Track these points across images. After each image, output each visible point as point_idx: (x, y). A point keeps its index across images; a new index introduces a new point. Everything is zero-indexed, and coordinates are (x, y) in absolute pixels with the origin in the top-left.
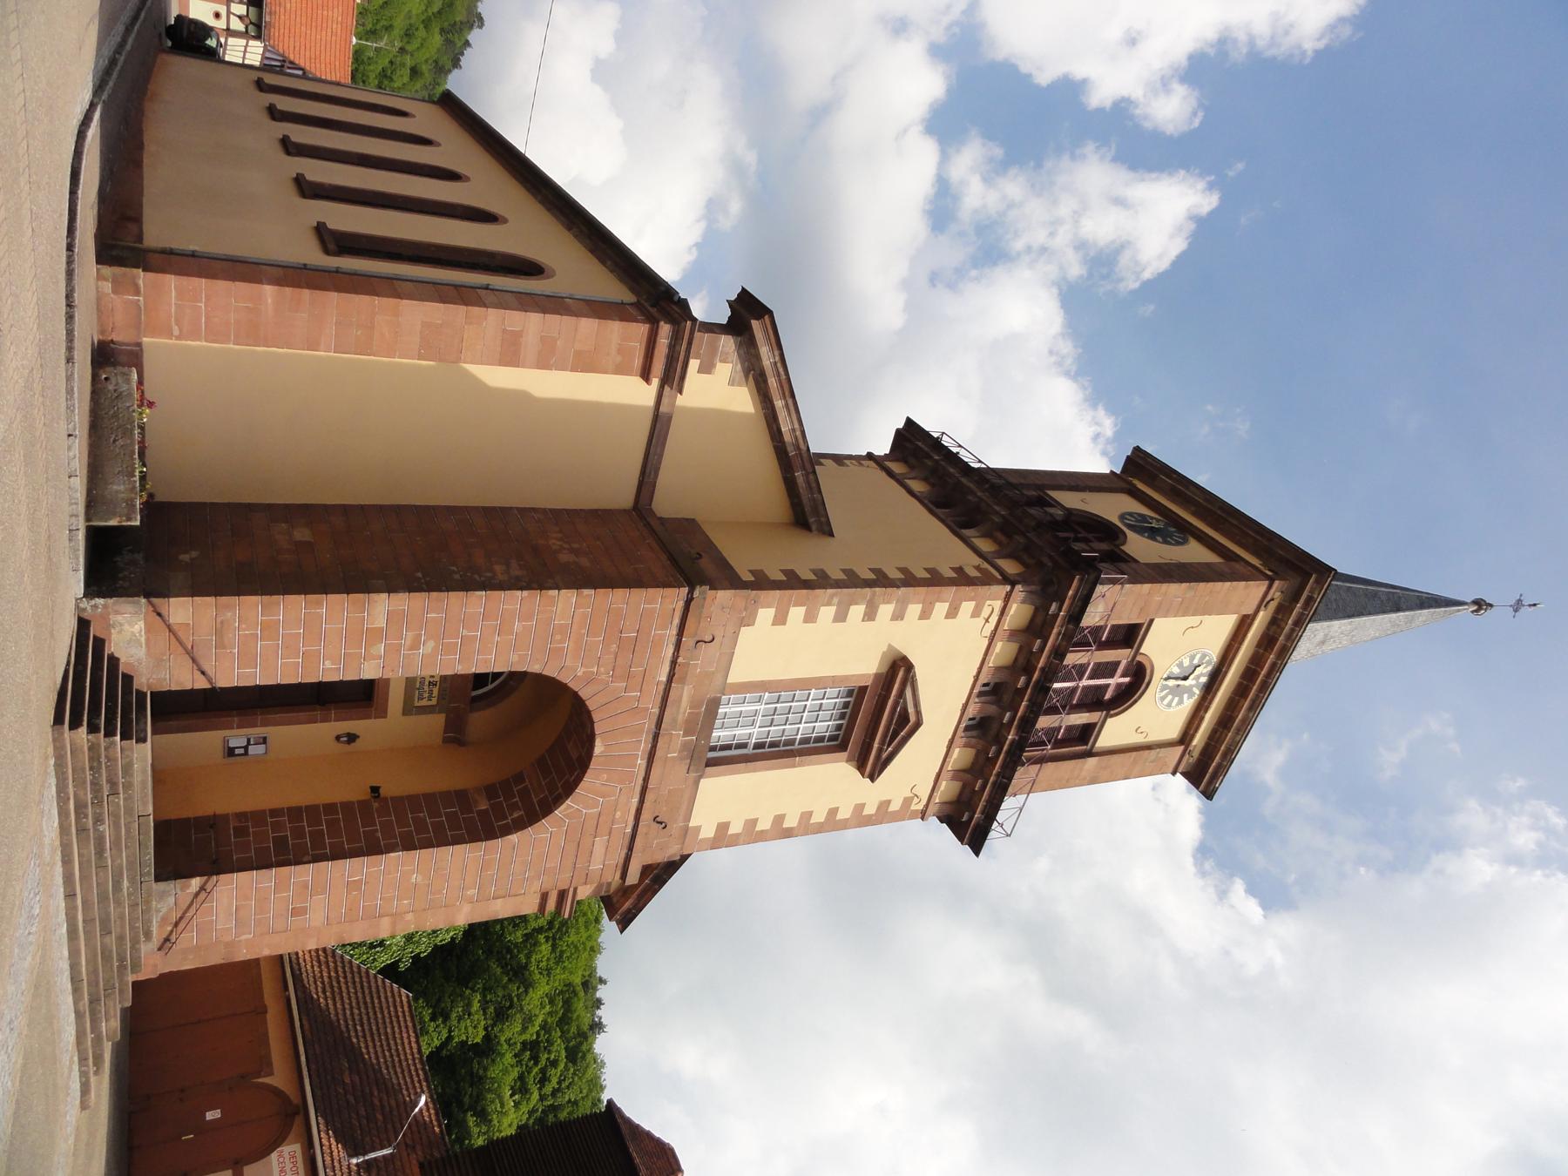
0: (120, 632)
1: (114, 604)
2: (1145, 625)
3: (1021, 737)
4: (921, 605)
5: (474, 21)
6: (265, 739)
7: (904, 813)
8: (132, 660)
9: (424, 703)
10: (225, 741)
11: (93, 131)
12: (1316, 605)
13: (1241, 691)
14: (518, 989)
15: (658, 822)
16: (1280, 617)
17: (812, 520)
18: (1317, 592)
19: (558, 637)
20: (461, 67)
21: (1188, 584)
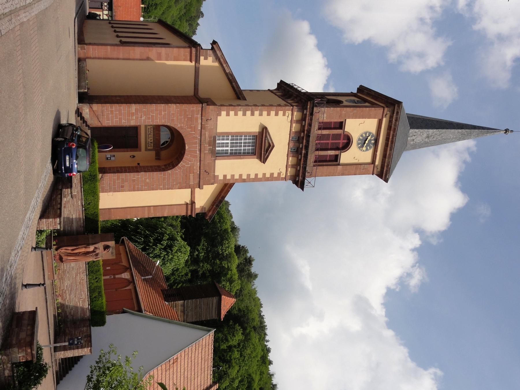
0: (84, 112)
1: (84, 105)
2: (344, 122)
3: (306, 152)
4: (266, 112)
5: (200, 15)
6: (114, 155)
7: (278, 178)
8: (87, 118)
9: (150, 148)
10: (106, 156)
11: (76, 20)
12: (399, 114)
13: (386, 145)
14: (226, 365)
16: (391, 120)
17: (240, 96)
18: (399, 110)
19: (173, 116)
20: (196, 34)
21: (353, 108)
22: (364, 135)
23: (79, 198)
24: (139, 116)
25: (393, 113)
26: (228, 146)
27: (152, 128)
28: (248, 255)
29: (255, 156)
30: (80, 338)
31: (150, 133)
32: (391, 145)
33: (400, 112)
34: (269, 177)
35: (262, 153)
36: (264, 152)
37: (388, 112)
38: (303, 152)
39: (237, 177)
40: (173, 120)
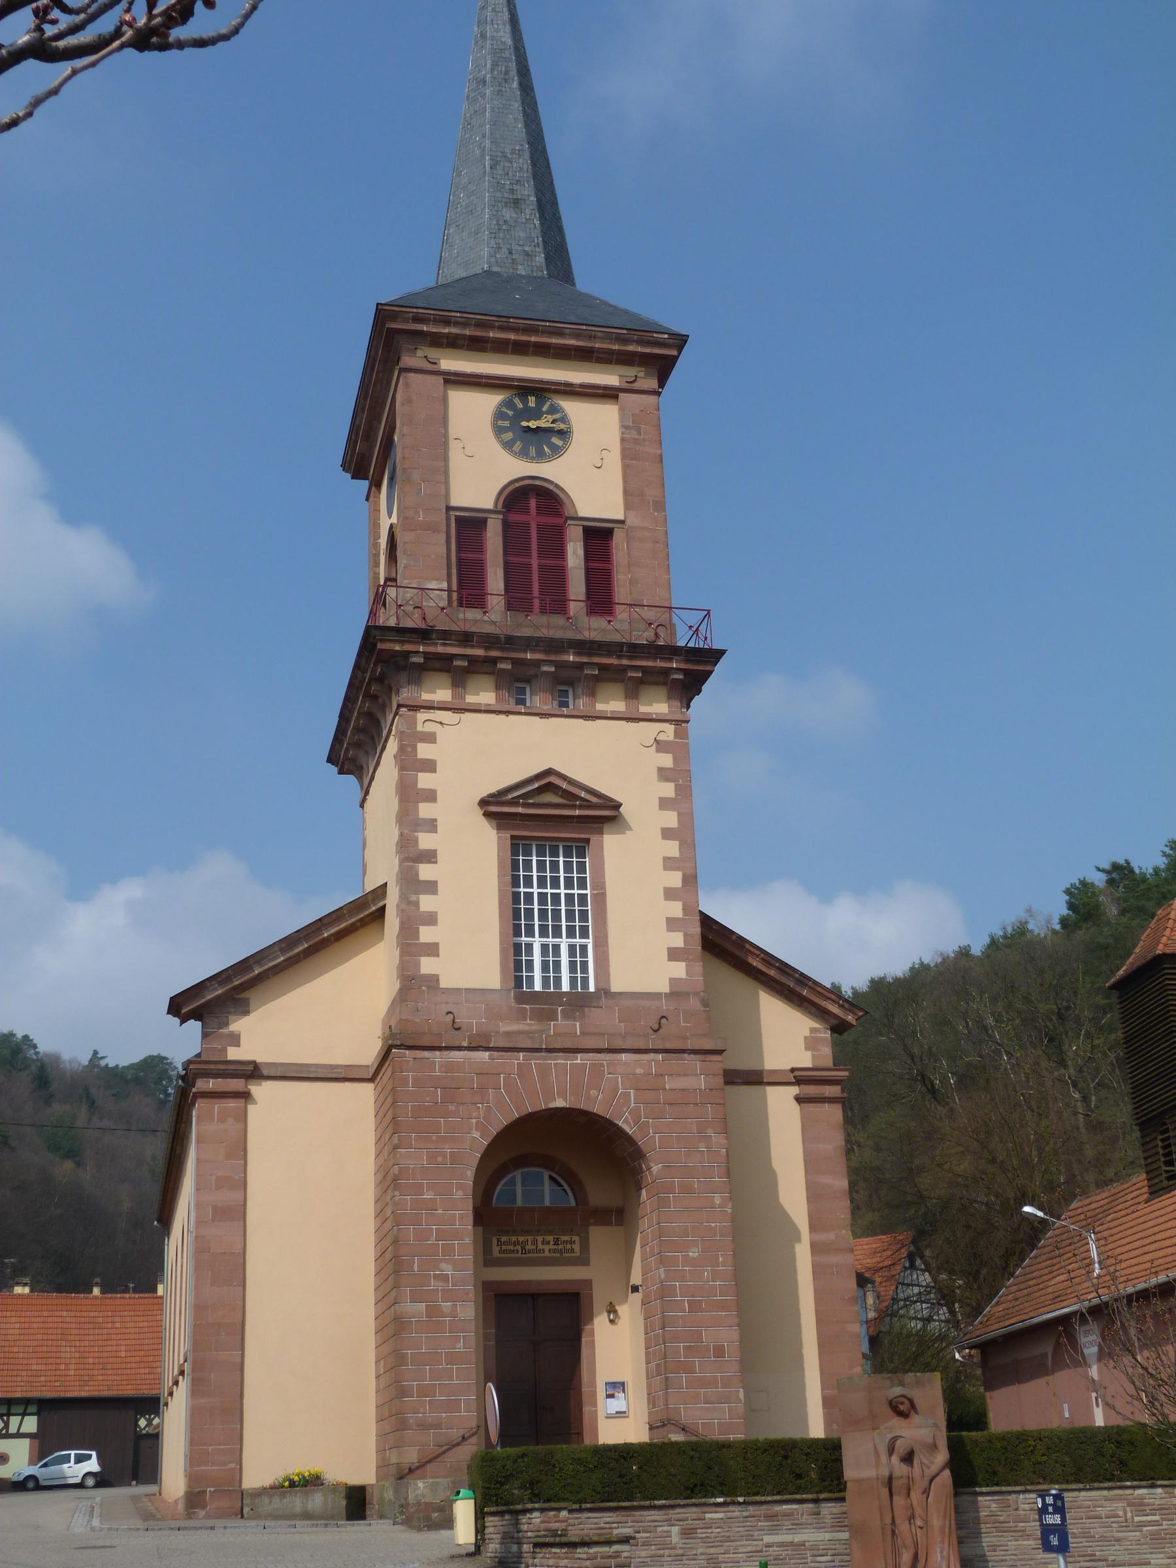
3: (570, 648)
4: (420, 805)
9: (577, 1247)
12: (421, 311)
15: (660, 1027)
16: (445, 341)
18: (406, 316)
19: (440, 1159)
22: (509, 436)
23: (695, 1516)
24: (440, 1285)
25: (421, 333)
26: (557, 948)
27: (498, 1240)
28: (1099, 880)
29: (594, 839)
30: (1039, 1500)
31: (519, 1248)
32: (543, 332)
33: (415, 310)
34: (676, 785)
35: (579, 817)
36: (574, 807)
37: (419, 353)
38: (571, 658)
39: (676, 909)
40: (455, 1158)
